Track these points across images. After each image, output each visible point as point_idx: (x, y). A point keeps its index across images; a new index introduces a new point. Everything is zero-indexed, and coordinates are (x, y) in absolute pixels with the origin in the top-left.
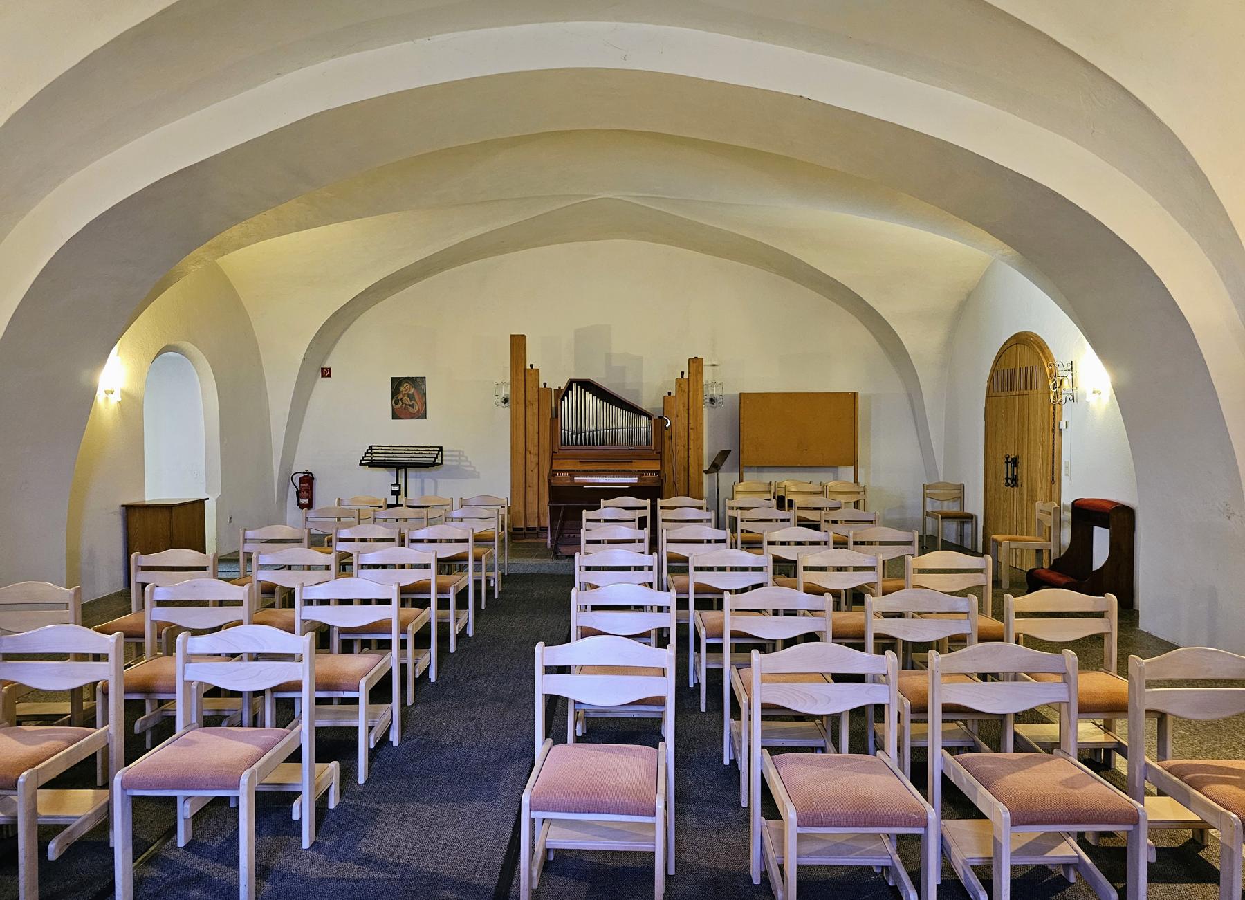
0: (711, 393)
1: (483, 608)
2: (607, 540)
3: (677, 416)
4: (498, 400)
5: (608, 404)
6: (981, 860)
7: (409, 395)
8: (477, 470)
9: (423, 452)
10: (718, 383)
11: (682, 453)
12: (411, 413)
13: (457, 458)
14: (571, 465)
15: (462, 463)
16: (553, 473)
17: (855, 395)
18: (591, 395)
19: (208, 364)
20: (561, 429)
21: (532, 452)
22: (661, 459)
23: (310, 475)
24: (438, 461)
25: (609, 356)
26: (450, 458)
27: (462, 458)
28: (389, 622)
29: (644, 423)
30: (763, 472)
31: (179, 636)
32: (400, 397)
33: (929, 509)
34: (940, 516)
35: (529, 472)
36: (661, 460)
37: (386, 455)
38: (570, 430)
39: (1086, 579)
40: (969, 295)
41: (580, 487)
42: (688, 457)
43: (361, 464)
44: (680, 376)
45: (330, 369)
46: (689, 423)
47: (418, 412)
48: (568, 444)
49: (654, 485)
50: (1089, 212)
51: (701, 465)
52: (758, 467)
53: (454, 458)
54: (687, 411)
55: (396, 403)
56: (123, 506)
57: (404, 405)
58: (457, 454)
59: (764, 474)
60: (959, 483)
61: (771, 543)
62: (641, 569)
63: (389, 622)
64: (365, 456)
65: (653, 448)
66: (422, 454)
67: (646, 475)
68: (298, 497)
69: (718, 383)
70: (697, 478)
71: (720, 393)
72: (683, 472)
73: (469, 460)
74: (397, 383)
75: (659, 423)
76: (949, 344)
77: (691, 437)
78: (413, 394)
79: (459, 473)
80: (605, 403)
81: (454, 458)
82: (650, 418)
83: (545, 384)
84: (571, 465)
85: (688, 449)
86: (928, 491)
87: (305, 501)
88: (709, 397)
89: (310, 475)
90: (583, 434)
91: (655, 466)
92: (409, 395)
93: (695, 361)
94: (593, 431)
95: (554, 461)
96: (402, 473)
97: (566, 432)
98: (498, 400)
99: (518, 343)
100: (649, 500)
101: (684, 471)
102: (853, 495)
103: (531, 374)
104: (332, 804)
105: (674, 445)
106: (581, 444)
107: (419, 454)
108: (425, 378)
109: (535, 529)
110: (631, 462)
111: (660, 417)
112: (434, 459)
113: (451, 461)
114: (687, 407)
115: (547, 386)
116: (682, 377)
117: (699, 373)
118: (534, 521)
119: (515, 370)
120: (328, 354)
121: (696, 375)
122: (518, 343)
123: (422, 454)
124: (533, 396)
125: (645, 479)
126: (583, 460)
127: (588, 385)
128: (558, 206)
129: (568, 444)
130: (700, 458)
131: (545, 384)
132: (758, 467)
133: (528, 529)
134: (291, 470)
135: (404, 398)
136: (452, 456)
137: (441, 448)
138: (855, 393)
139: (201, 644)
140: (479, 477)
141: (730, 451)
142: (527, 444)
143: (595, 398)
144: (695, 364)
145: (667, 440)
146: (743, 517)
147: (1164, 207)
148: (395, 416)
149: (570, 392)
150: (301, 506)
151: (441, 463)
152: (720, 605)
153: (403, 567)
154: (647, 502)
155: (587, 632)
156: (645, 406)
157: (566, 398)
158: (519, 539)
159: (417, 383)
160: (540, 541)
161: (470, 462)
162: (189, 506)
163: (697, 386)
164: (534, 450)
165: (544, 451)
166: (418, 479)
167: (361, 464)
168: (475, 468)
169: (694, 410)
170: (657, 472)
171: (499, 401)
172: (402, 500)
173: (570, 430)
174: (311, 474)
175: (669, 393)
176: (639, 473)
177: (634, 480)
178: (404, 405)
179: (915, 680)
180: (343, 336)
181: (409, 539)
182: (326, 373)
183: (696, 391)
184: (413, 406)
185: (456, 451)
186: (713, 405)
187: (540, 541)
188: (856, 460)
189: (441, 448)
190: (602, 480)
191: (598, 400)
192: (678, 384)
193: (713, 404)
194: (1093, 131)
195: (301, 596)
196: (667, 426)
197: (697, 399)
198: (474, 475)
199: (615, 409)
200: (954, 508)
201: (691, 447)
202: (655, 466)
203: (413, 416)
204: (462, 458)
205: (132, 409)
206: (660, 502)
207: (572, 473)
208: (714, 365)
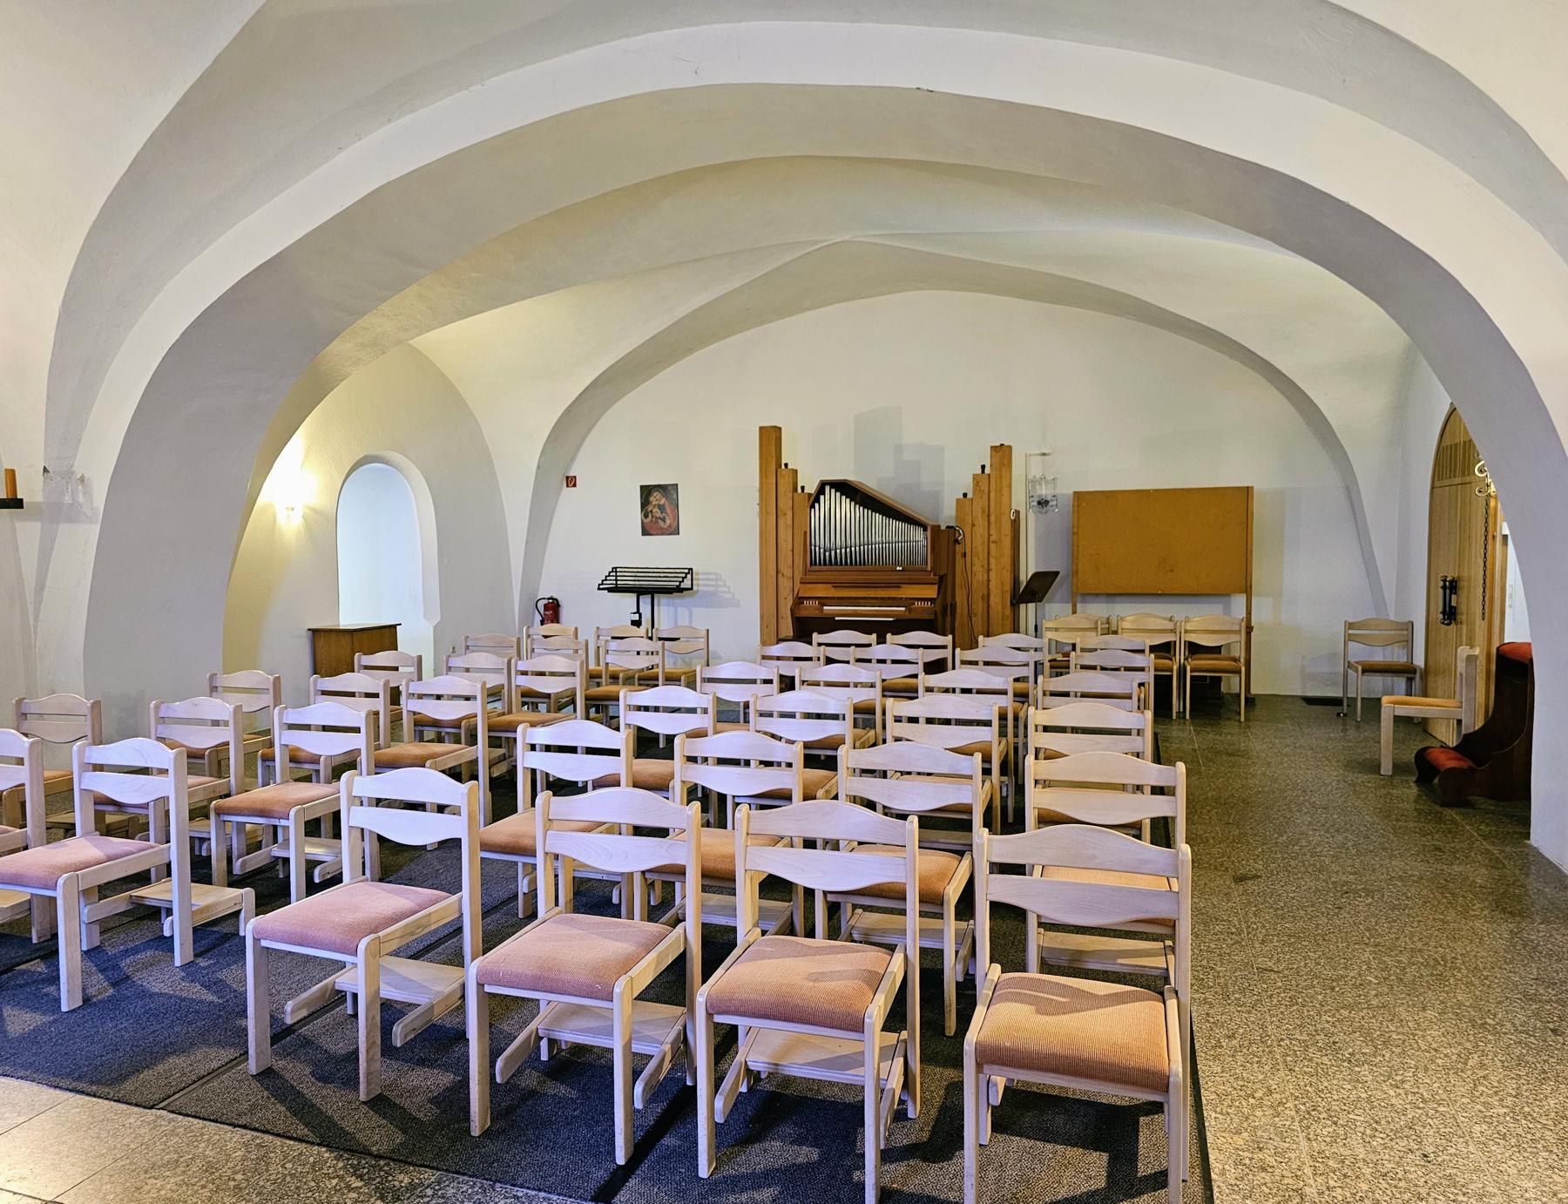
0: (1038, 492)
2: (825, 682)
3: (973, 525)
5: (870, 512)
6: (767, 1065)
10: (1050, 478)
11: (980, 576)
12: (662, 529)
13: (714, 583)
16: (799, 600)
17: (1248, 490)
19: (422, 478)
20: (811, 546)
27: (719, 583)
28: (968, 810)
29: (918, 535)
30: (1113, 602)
31: (343, 775)
32: (649, 509)
34: (1360, 668)
37: (636, 578)
38: (822, 546)
39: (1484, 765)
42: (989, 581)
43: (599, 589)
45: (575, 477)
46: (989, 535)
47: (670, 526)
48: (820, 564)
50: (1351, 204)
54: (986, 518)
55: (646, 516)
56: (309, 630)
58: (714, 577)
60: (1406, 620)
61: (769, 682)
62: (693, 711)
63: (968, 810)
64: (609, 576)
65: (929, 569)
67: (917, 604)
69: (1050, 478)
70: (1000, 609)
72: (981, 602)
73: (727, 584)
74: (646, 492)
75: (945, 540)
78: (664, 505)
79: (712, 600)
80: (866, 510)
85: (989, 570)
88: (1037, 499)
90: (838, 551)
94: (851, 547)
97: (817, 548)
99: (771, 438)
102: (1220, 636)
103: (784, 476)
105: (968, 565)
106: (836, 564)
108: (677, 485)
110: (899, 587)
112: (678, 583)
114: (986, 513)
115: (805, 491)
116: (983, 472)
117: (1004, 465)
120: (572, 460)
122: (771, 438)
127: (844, 488)
128: (787, 259)
136: (708, 579)
137: (692, 569)
138: (1248, 487)
140: (739, 606)
141: (1056, 574)
142: (779, 565)
144: (998, 454)
145: (958, 557)
147: (1479, 181)
148: (645, 532)
149: (822, 497)
151: (692, 589)
152: (668, 754)
153: (439, 697)
155: (1048, 819)
157: (817, 505)
159: (669, 491)
162: (333, 636)
166: (671, 608)
167: (599, 589)
168: (733, 594)
169: (996, 517)
173: (822, 546)
174: (556, 600)
175: (965, 495)
179: (715, 841)
180: (588, 439)
181: (702, 678)
182: (571, 481)
183: (999, 491)
184: (664, 520)
185: (714, 574)
188: (1248, 584)
189: (692, 569)
191: (857, 506)
194: (1344, 81)
195: (524, 739)
201: (993, 566)
202: (932, 592)
204: (719, 583)
205: (322, 532)
207: (824, 601)
208: (1044, 454)
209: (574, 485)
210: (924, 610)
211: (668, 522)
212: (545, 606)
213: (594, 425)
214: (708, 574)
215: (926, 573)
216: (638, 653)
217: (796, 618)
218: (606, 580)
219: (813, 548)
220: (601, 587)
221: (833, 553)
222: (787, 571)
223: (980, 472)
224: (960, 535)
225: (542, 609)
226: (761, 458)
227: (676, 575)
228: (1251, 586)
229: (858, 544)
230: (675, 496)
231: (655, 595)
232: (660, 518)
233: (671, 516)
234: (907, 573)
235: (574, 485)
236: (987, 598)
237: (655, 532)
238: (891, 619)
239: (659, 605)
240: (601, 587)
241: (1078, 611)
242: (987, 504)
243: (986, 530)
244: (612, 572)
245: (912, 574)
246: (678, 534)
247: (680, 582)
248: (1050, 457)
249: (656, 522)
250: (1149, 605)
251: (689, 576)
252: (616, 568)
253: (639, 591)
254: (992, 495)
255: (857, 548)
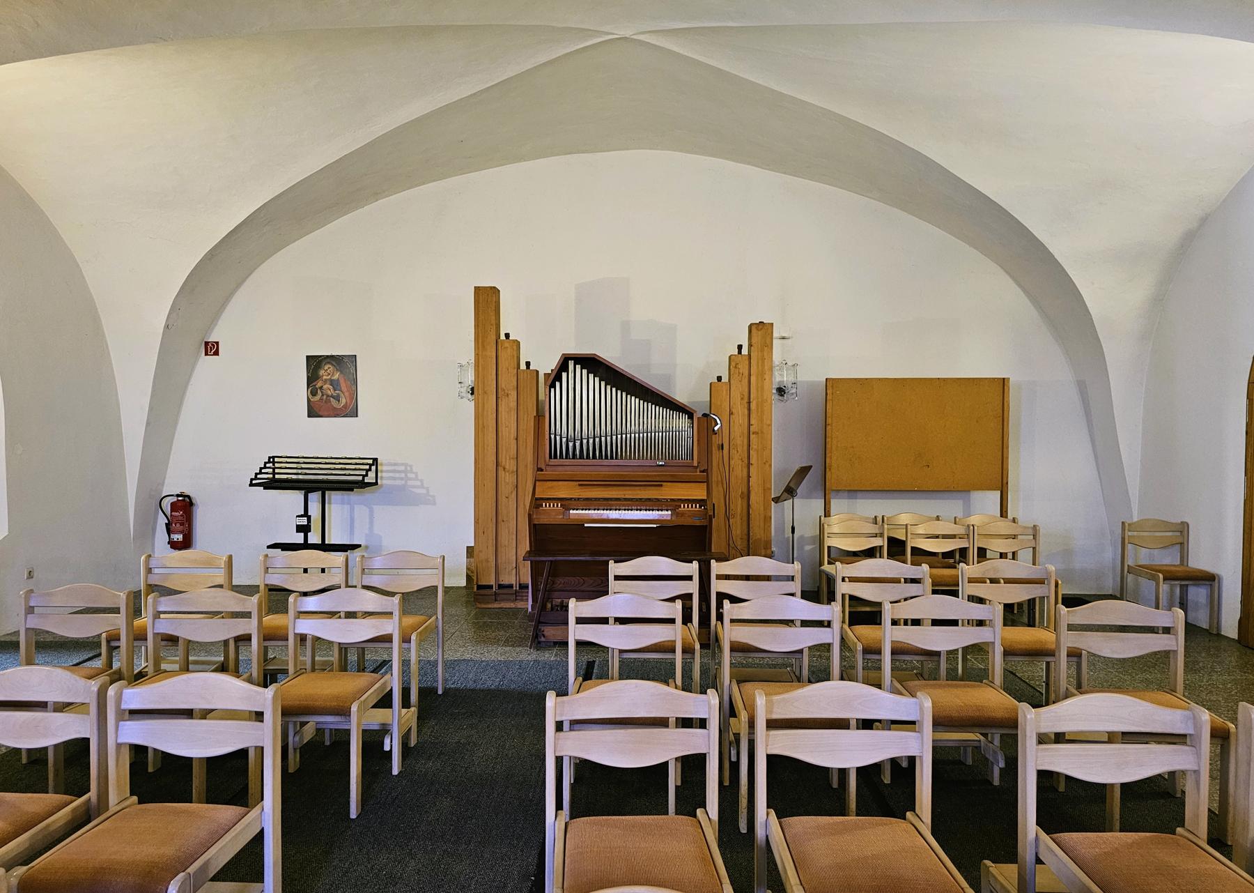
1: (353, 815)
3: (731, 413)
4: (462, 390)
7: (332, 382)
8: (431, 493)
9: (347, 467)
10: (790, 364)
11: (739, 470)
14: (564, 490)
15: (410, 483)
16: (537, 503)
17: (1004, 381)
18: (597, 379)
20: (550, 434)
21: (507, 467)
22: (707, 481)
23: (187, 500)
24: (370, 478)
25: (626, 326)
26: (391, 474)
29: (681, 422)
32: (319, 385)
33: (1130, 562)
34: (1161, 576)
35: (502, 499)
36: (707, 482)
38: (564, 435)
40: (1204, 221)
41: (578, 527)
43: (251, 485)
44: (736, 352)
45: (217, 343)
46: (749, 425)
47: (345, 406)
48: (561, 457)
49: (698, 523)
51: (766, 490)
52: (849, 491)
53: (397, 475)
54: (746, 405)
55: (314, 393)
57: (325, 397)
58: (402, 468)
59: (858, 500)
60: (1179, 521)
65: (695, 464)
66: (345, 469)
68: (169, 532)
69: (790, 364)
70: (762, 508)
71: (792, 379)
74: (314, 364)
76: (1159, 301)
77: (754, 445)
79: (403, 496)
81: (397, 475)
82: (691, 416)
83: (528, 364)
84: (564, 490)
85: (749, 464)
86: (1130, 533)
87: (178, 537)
88: (775, 386)
89: (187, 500)
90: (585, 441)
91: (699, 492)
92: (332, 382)
93: (760, 327)
95: (537, 483)
96: (314, 498)
97: (558, 438)
98: (462, 390)
99: (487, 300)
100: (695, 565)
101: (742, 498)
103: (507, 348)
104: (413, 743)
106: (581, 457)
107: (341, 469)
109: (511, 586)
110: (661, 485)
111: (705, 415)
112: (360, 478)
113: (394, 479)
114: (746, 400)
116: (740, 352)
118: (510, 573)
119: (480, 341)
121: (762, 351)
122: (487, 300)
123: (345, 469)
124: (508, 381)
125: (683, 514)
126: (584, 483)
127: (591, 364)
129: (561, 457)
130: (766, 480)
131: (528, 364)
132: (849, 491)
133: (501, 586)
134: (162, 491)
135: (325, 387)
136: (394, 471)
137: (375, 460)
138: (1004, 379)
139: (311, 603)
140: (434, 504)
141: (811, 466)
143: (603, 384)
145: (715, 449)
146: (896, 617)
148: (312, 414)
149: (564, 375)
150: (174, 545)
151: (376, 483)
154: (693, 568)
156: (681, 397)
157: (558, 384)
158: (488, 603)
159: (345, 363)
160: (520, 605)
161: (422, 481)
163: (763, 365)
164: (510, 464)
165: (526, 466)
167: (251, 485)
168: (427, 489)
169: (757, 405)
170: (702, 502)
171: (464, 390)
172: (314, 538)
173: (564, 435)
174: (189, 497)
175: (719, 379)
176: (673, 504)
177: (666, 514)
178: (325, 397)
182: (212, 349)
184: (337, 398)
185: (402, 464)
186: (781, 398)
187: (520, 605)
188: (1005, 481)
189: (375, 460)
190: (614, 514)
192: (733, 364)
193: (782, 395)
196: (716, 428)
197: (762, 388)
198: (428, 500)
199: (634, 402)
200: (1168, 559)
202: (699, 492)
203: (339, 413)
206: (716, 568)
207: (567, 504)
208: (784, 338)
209: (216, 353)
210: (694, 514)
211: (343, 401)
212: (173, 504)
213: (244, 281)
214: (395, 464)
215: (691, 469)
216: (306, 571)
217: (535, 525)
218: (261, 473)
219: (553, 436)
220: (254, 482)
221: (578, 444)
222: (510, 464)
223: (737, 353)
224: (717, 424)
225: (168, 510)
226: (477, 326)
227: (358, 467)
228: (1007, 483)
229: (614, 432)
230: (352, 371)
231: (327, 492)
232: (332, 396)
233: (347, 394)
234: (669, 468)
235: (216, 353)
236: (747, 496)
237: (326, 413)
238: (655, 526)
239: (330, 503)
240: (254, 482)
241: (832, 512)
242: (747, 390)
243: (746, 420)
244: (269, 462)
245: (677, 471)
246: (357, 416)
247: (364, 476)
248: (790, 340)
249: (328, 401)
250: (922, 501)
251: (374, 468)
252: (274, 457)
253: (306, 487)
254: (753, 379)
255: (609, 438)
